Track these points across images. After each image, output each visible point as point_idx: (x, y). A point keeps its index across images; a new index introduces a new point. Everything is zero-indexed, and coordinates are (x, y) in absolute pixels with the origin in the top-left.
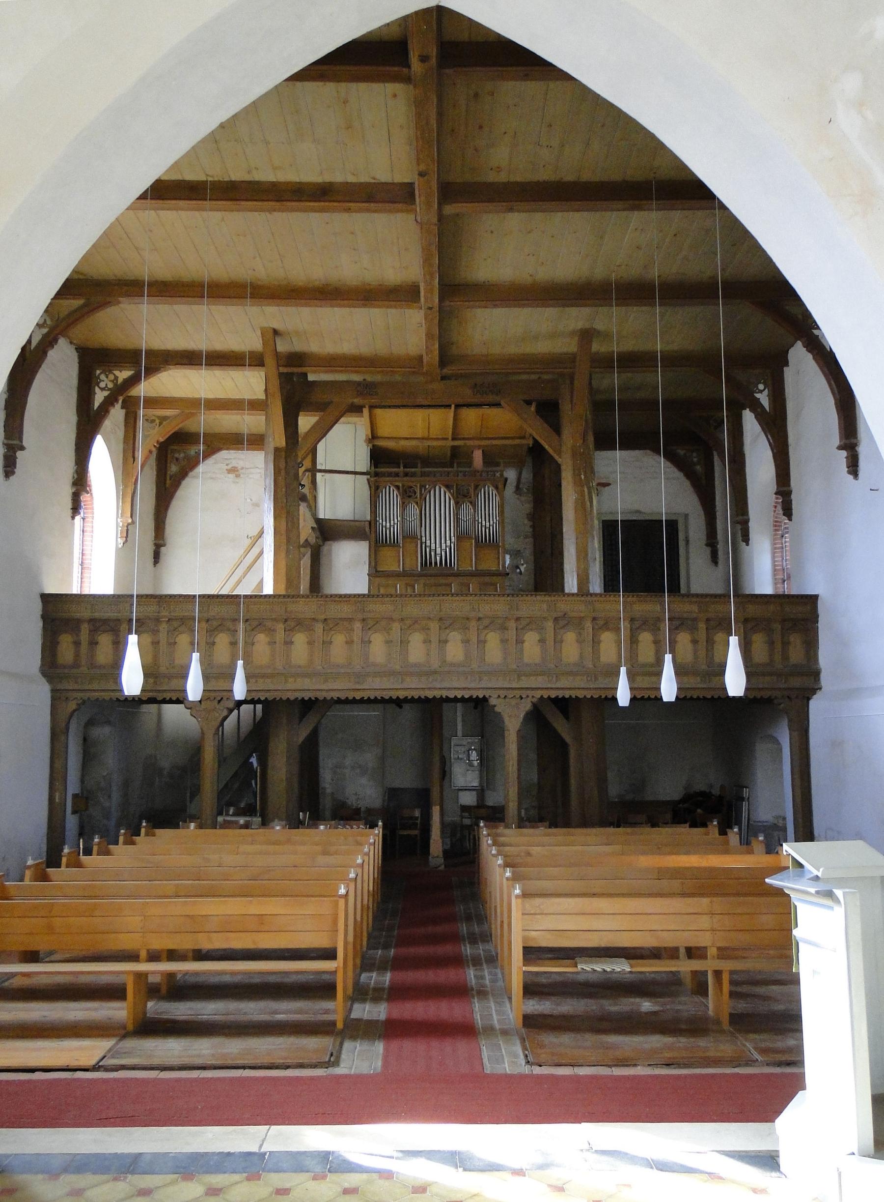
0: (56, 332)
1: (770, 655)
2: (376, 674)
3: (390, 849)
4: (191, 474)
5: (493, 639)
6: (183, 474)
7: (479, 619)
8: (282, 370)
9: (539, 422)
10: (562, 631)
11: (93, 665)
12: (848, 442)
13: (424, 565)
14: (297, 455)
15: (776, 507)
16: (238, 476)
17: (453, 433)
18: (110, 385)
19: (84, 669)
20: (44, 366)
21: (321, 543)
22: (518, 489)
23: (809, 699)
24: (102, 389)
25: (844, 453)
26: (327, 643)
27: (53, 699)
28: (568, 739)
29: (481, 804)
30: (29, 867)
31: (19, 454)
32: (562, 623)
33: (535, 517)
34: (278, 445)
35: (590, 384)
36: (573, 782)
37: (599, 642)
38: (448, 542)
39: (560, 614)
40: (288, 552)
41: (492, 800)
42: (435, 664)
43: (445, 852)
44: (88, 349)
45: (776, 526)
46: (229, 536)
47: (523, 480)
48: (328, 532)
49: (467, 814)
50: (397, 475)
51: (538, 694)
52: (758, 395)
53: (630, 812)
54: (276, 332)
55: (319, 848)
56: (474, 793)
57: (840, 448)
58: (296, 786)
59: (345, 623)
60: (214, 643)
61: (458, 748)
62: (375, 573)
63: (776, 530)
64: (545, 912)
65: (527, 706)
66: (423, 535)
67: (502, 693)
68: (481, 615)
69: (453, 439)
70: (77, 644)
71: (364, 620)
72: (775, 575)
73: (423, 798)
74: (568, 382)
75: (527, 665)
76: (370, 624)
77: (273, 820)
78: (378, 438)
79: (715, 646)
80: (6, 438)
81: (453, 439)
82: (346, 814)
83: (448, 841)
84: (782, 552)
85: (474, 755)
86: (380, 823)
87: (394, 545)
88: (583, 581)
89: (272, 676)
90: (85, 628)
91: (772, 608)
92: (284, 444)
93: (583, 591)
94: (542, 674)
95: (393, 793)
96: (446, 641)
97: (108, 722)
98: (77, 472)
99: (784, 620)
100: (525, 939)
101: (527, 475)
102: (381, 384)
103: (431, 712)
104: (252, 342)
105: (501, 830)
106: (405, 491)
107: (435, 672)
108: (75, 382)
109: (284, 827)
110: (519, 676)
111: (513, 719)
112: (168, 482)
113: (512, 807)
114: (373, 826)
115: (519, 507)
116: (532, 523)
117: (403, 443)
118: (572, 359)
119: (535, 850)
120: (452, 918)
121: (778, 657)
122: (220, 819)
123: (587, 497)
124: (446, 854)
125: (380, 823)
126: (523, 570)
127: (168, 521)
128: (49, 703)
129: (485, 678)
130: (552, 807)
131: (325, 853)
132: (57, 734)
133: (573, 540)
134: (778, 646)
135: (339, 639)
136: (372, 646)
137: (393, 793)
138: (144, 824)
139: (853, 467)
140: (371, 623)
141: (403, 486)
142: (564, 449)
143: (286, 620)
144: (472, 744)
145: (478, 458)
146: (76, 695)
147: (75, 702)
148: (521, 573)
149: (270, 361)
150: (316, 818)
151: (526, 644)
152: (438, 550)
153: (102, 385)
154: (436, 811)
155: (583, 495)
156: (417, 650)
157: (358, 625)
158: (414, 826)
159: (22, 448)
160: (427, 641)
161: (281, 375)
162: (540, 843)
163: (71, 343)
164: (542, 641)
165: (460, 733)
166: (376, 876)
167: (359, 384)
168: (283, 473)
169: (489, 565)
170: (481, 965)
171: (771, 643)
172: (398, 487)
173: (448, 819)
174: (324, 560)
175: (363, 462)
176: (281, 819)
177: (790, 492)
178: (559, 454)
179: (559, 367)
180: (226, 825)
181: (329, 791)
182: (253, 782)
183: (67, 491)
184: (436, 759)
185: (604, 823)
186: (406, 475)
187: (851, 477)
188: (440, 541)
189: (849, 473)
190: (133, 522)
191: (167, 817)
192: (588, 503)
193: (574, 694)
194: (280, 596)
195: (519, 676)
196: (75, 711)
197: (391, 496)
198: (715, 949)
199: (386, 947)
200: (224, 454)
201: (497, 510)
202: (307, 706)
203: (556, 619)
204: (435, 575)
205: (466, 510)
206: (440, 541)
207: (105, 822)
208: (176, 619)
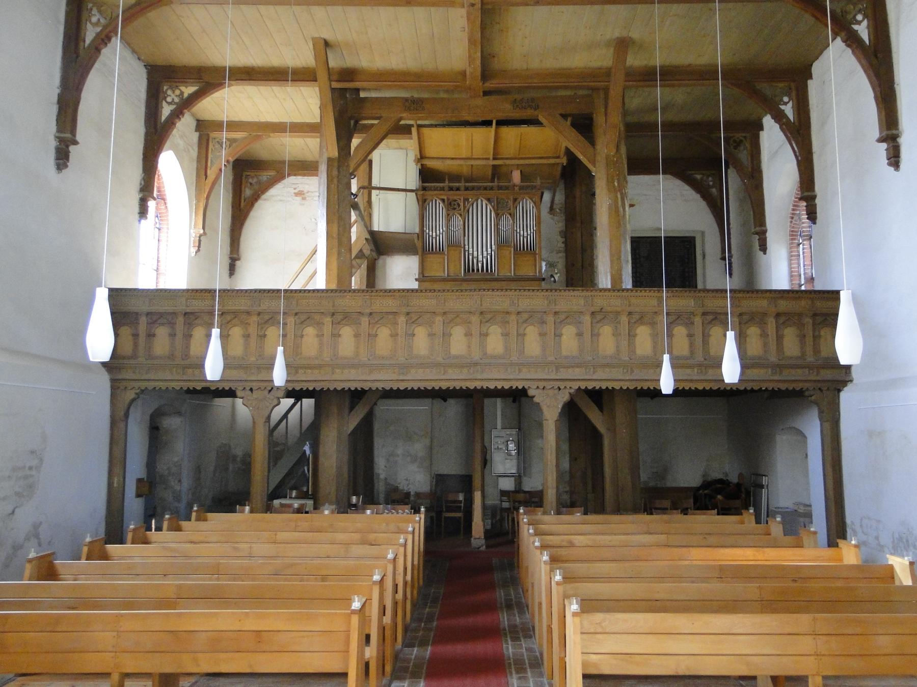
0: (107, 30)
1: (802, 348)
2: (422, 366)
3: (431, 533)
4: (264, 197)
5: (532, 332)
6: (256, 198)
8: (335, 85)
9: (573, 133)
10: (599, 325)
11: (150, 356)
12: (890, 132)
13: (467, 270)
14: (348, 166)
15: (792, 218)
16: (304, 199)
18: (177, 100)
19: (141, 360)
20: (96, 65)
22: (552, 208)
23: (839, 391)
24: (169, 103)
25: (884, 146)
26: (372, 336)
27: (112, 388)
28: (601, 427)
29: (518, 490)
30: (30, 561)
31: (72, 148)
32: (599, 317)
33: (566, 234)
34: (331, 155)
35: (624, 103)
36: (608, 471)
37: (635, 335)
38: (489, 250)
39: (598, 309)
40: (339, 254)
41: (529, 485)
42: (476, 356)
43: (487, 532)
44: (156, 66)
45: (792, 235)
46: (292, 243)
48: (381, 245)
49: (505, 498)
50: (442, 189)
51: (576, 385)
52: (782, 107)
53: (656, 498)
54: (327, 44)
55: (356, 536)
56: (513, 479)
57: (880, 140)
58: (345, 469)
59: (391, 316)
60: (265, 336)
61: (498, 440)
62: (422, 278)
63: (792, 239)
64: (607, 631)
65: (565, 397)
67: (541, 384)
69: (494, 159)
70: (136, 336)
71: (408, 314)
72: (791, 281)
73: (466, 483)
74: (602, 95)
75: (566, 357)
76: (414, 318)
77: (324, 505)
79: (748, 339)
80: (59, 131)
81: (494, 159)
82: (398, 498)
83: (489, 521)
84: (799, 259)
85: (512, 446)
86: (423, 509)
87: (440, 252)
88: (616, 279)
89: (320, 367)
90: (143, 320)
91: (803, 303)
92: (336, 154)
93: (616, 287)
94: (578, 366)
95: (440, 479)
96: (487, 335)
97: (179, 413)
98: (144, 179)
99: (815, 315)
100: (585, 664)
101: (560, 197)
102: (426, 99)
103: (473, 400)
104: (305, 57)
105: (539, 515)
106: (450, 204)
107: (476, 364)
108: (143, 95)
109: (332, 512)
110: (557, 368)
111: (550, 409)
112: (243, 204)
113: (551, 495)
114: (417, 511)
115: (553, 226)
117: (449, 162)
118: (607, 73)
119: (579, 540)
120: (491, 607)
121: (809, 350)
122: (276, 502)
123: (620, 203)
124: (488, 534)
125: (423, 509)
127: (242, 239)
128: (109, 392)
129: (524, 370)
130: (587, 493)
131: (364, 542)
132: (118, 422)
133: (607, 242)
134: (809, 340)
135: (384, 333)
136: (415, 338)
137: (440, 479)
138: (195, 508)
139: (894, 159)
140: (414, 317)
141: (448, 199)
142: (598, 158)
143: (333, 314)
144: (511, 435)
145: (516, 177)
146: (136, 385)
147: (134, 391)
148: (555, 281)
149: (322, 75)
150: (370, 499)
151: (564, 338)
153: (169, 99)
154: (477, 496)
155: (616, 202)
156: (459, 343)
157: (402, 319)
158: (458, 509)
159: (75, 143)
160: (468, 334)
161: (333, 90)
162: (582, 532)
163: (139, 59)
164: (580, 335)
165: (499, 426)
166: (416, 562)
167: (406, 100)
168: (335, 181)
169: (527, 270)
170: (525, 670)
171: (802, 337)
172: (443, 200)
173: (489, 502)
174: (378, 273)
175: (413, 181)
176: (331, 503)
177: (814, 197)
178: (594, 164)
179: (594, 83)
180: (284, 509)
181: (382, 476)
182: (306, 468)
183: (135, 197)
184: (478, 447)
185: (635, 510)
186: (451, 189)
187: (892, 169)
188: (481, 247)
189: (890, 164)
190: (205, 234)
191: (227, 501)
192: (621, 209)
193: (610, 385)
194: (332, 291)
195: (557, 368)
196: (133, 400)
197: (438, 209)
198: (820, 678)
199: (423, 643)
200: (291, 180)
201: (536, 221)
202: (356, 396)
203: (593, 314)
204: (476, 278)
205: (506, 222)
206: (481, 247)
207: (176, 504)
208: (228, 312)
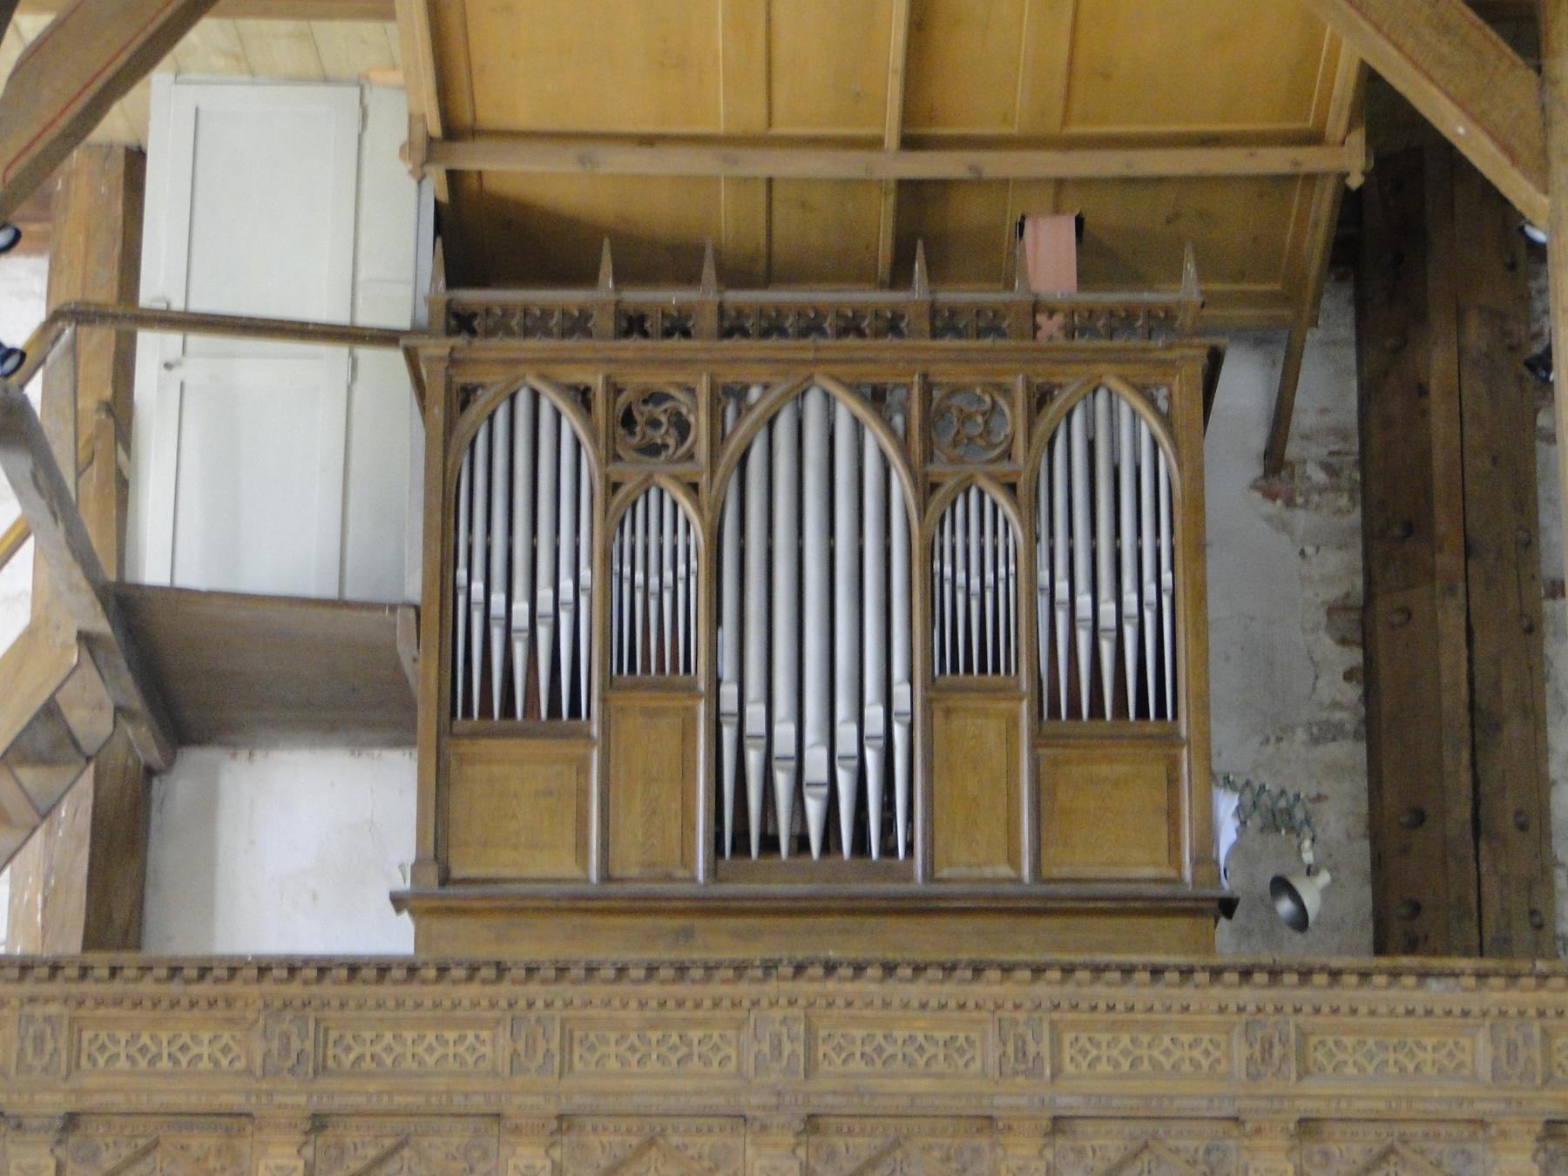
7: (1059, 1124)
13: (734, 840)
17: (910, 111)
21: (154, 756)
38: (874, 714)
47: (1305, 416)
50: (577, 325)
62: (439, 888)
66: (727, 669)
68: (1066, 1102)
71: (318, 1123)
78: (474, 133)
81: (910, 143)
87: (564, 712)
101: (1328, 391)
116: (1355, 657)
126: (1312, 901)
141: (615, 389)
145: (1050, 258)
148: (1300, 921)
152: (816, 758)
172: (583, 398)
174: (167, 855)
175: (394, 271)
186: (633, 324)
188: (822, 692)
205: (986, 535)
206: (822, 692)
